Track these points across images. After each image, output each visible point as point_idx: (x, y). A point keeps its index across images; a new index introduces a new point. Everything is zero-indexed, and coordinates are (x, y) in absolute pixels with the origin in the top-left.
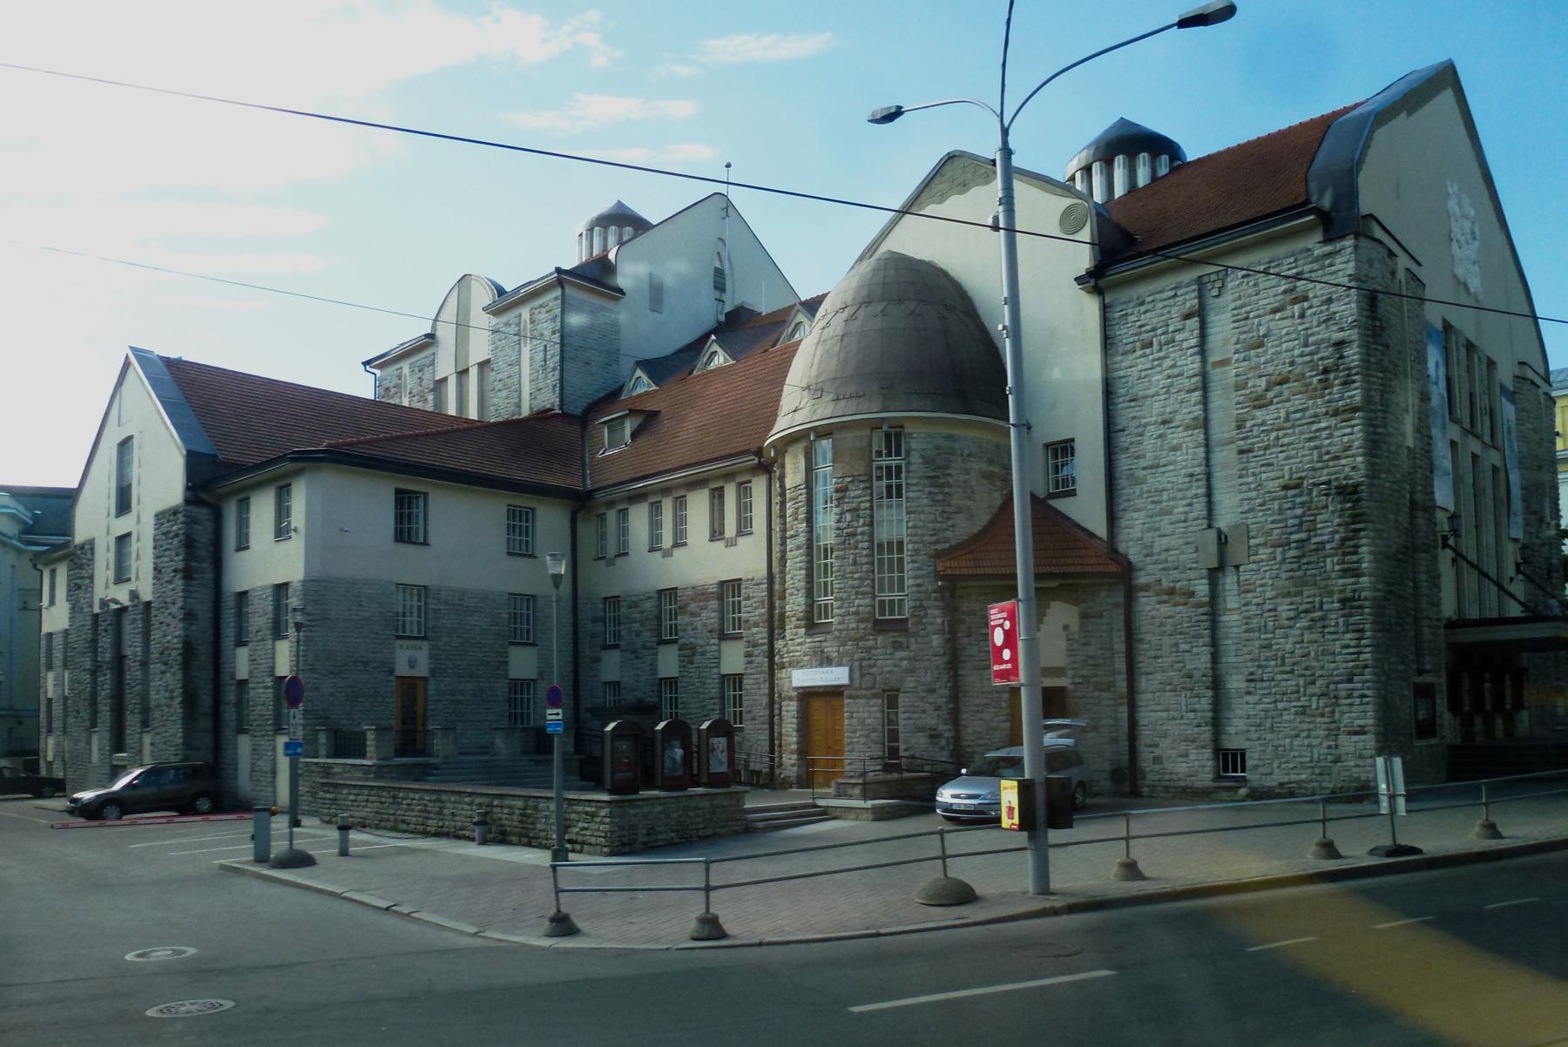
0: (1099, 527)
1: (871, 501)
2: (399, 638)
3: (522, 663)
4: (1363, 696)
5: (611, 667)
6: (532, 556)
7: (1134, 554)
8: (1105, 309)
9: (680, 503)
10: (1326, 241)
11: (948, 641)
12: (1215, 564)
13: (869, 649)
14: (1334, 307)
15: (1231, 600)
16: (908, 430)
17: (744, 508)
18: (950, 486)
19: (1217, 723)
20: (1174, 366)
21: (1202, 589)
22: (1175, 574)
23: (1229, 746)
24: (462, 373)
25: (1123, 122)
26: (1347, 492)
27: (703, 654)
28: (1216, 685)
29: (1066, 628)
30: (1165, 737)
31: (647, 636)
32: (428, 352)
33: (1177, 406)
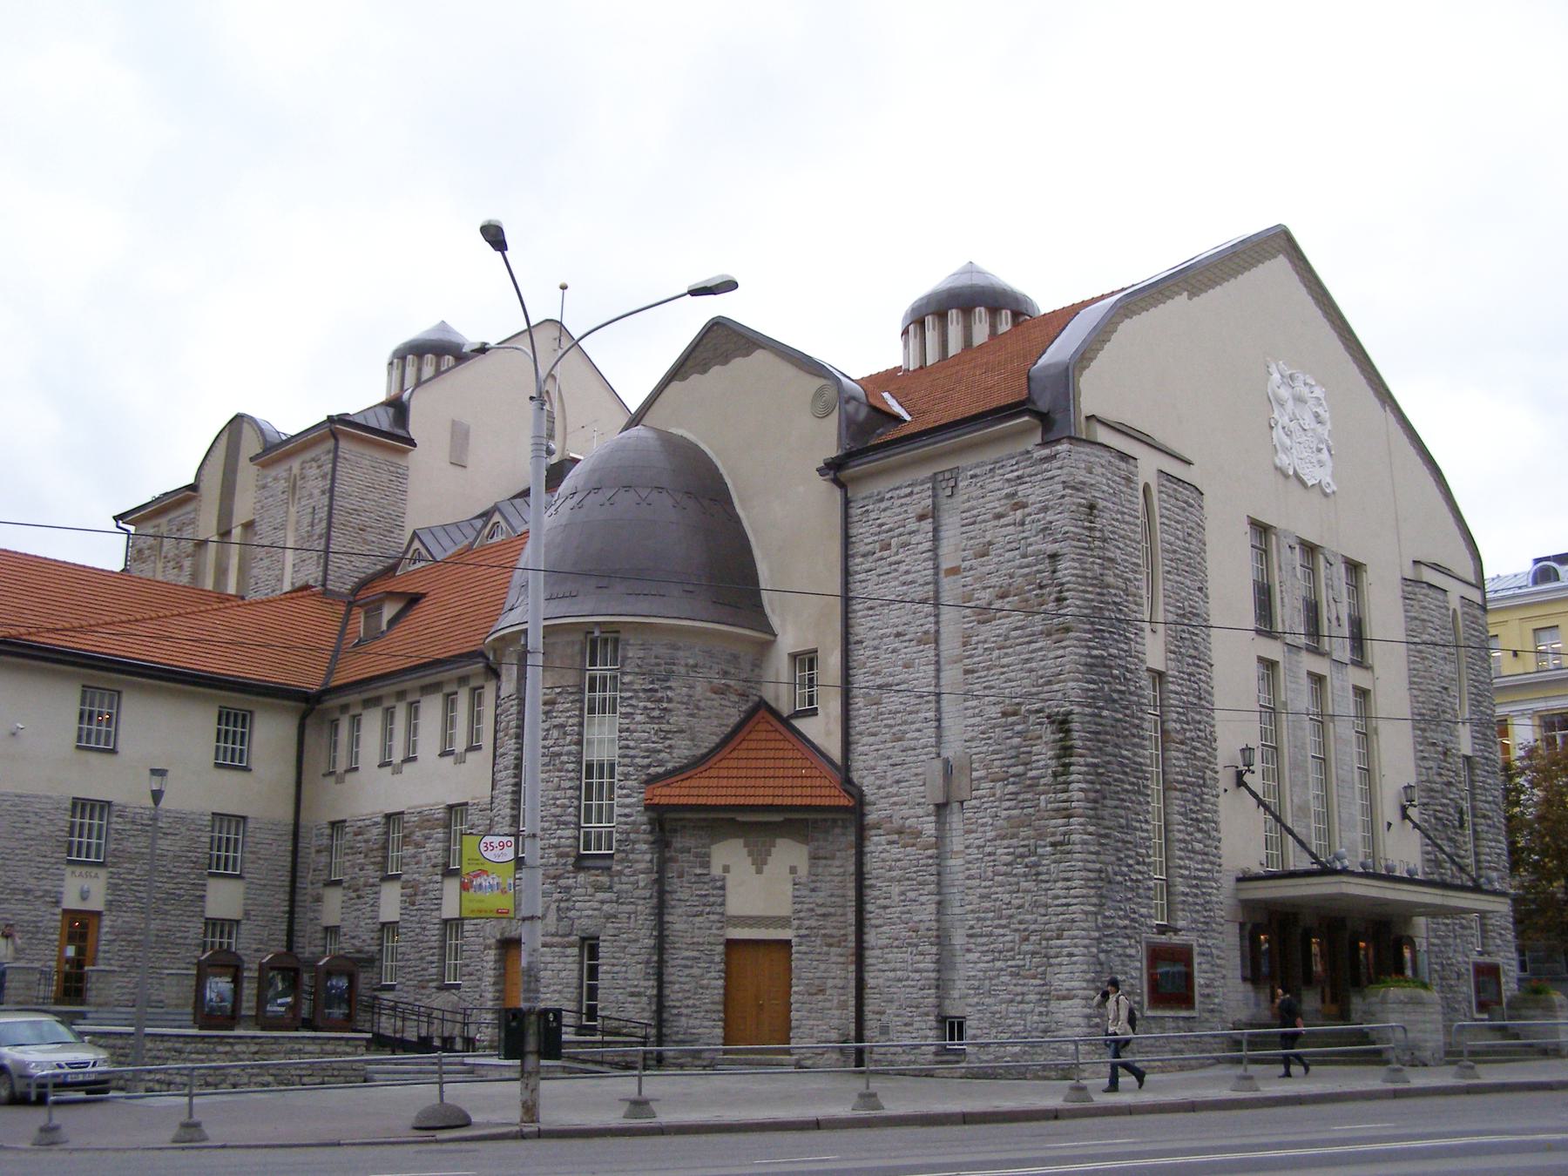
0: (835, 752)
1: (581, 716)
2: (70, 862)
3: (224, 899)
4: (1070, 955)
5: (332, 908)
6: (247, 769)
7: (868, 783)
8: (847, 503)
9: (414, 709)
10: (1045, 444)
11: (656, 881)
12: (941, 800)
13: (568, 889)
14: (1050, 516)
15: (957, 843)
16: (622, 636)
17: (475, 717)
18: (670, 700)
19: (941, 986)
20: (907, 572)
21: (929, 828)
22: (906, 812)
23: (953, 1013)
24: (225, 534)
25: (971, 268)
26: (1062, 723)
27: (425, 893)
28: (942, 939)
29: (793, 870)
30: (891, 1001)
31: (372, 873)
32: (190, 507)
33: (909, 618)
